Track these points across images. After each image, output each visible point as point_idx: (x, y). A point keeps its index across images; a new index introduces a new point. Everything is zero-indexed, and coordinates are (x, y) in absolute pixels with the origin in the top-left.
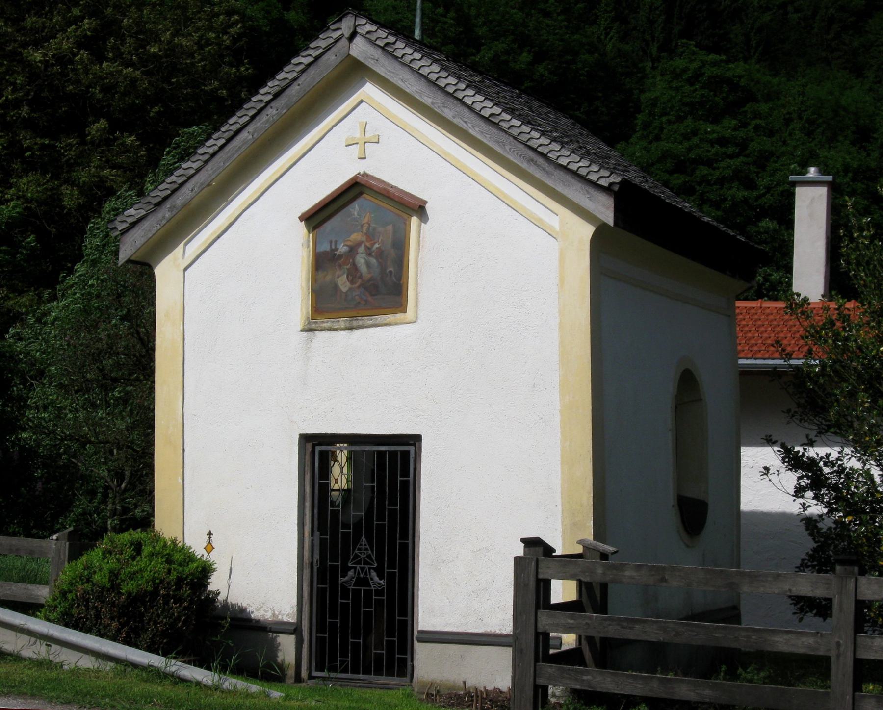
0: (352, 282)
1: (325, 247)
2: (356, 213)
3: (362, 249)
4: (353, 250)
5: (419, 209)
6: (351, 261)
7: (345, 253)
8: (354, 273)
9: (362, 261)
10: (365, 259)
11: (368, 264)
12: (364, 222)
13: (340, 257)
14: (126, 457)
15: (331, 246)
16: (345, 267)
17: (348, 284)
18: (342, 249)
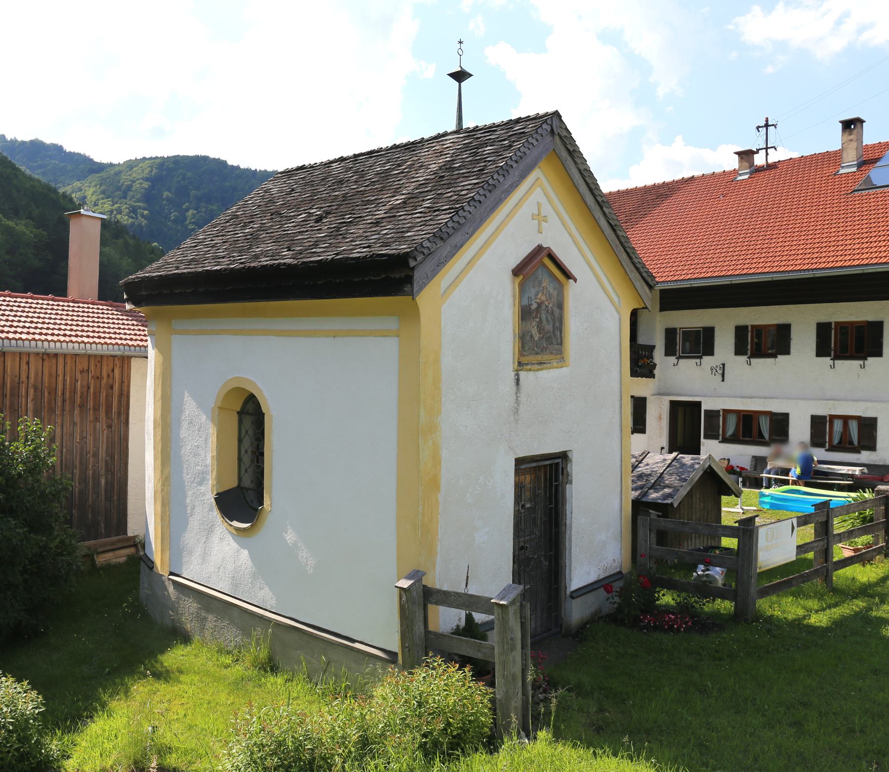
9: (544, 316)
18: (534, 306)
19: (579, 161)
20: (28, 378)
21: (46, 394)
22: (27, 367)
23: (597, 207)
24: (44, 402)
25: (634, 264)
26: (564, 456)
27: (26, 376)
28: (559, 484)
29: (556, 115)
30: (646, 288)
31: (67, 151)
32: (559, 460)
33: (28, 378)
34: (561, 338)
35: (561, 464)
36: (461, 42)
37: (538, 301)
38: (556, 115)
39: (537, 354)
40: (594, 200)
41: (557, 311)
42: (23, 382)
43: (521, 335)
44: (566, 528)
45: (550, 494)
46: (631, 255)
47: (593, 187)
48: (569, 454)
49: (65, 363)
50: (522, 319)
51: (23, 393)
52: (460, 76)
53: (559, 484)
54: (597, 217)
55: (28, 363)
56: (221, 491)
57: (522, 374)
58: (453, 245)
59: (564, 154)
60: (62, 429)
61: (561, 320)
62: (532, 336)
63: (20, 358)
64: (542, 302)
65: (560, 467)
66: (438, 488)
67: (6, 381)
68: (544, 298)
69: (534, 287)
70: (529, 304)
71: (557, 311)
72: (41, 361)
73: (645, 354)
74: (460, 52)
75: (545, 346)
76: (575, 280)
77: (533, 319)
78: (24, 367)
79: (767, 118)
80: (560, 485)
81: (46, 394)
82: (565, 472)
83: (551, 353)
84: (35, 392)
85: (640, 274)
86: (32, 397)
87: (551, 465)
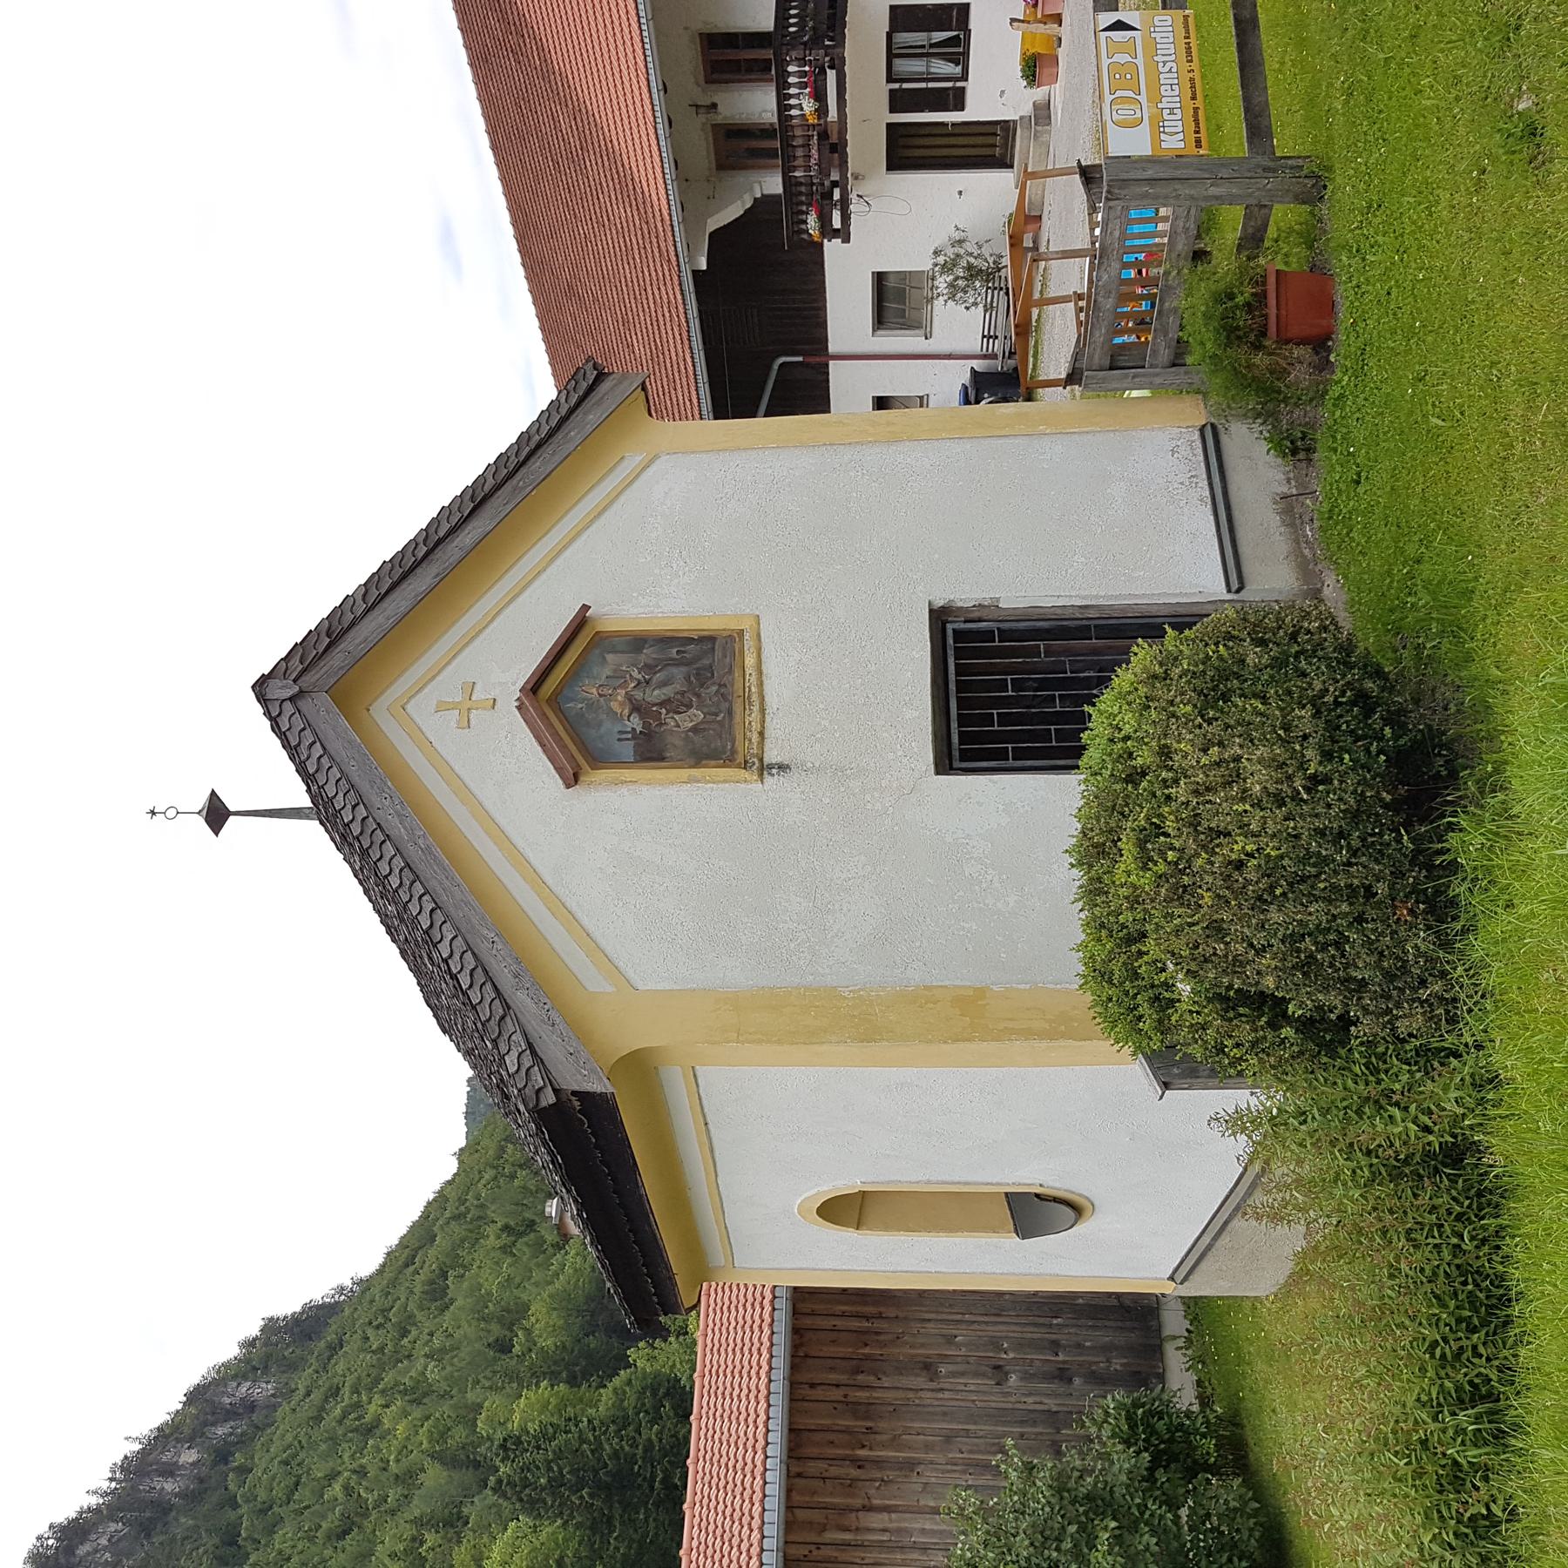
0: (689, 706)
1: (627, 750)
2: (580, 706)
3: (638, 695)
4: (636, 708)
5: (580, 622)
6: (654, 709)
7: (641, 719)
8: (676, 705)
9: (656, 692)
10: (654, 690)
11: (664, 684)
12: (596, 693)
13: (646, 725)
15: (628, 739)
16: (663, 716)
17: (693, 711)
18: (636, 723)
19: (349, 617)
20: (837, 1386)
21: (867, 1351)
22: (819, 1388)
23: (438, 553)
24: (882, 1355)
25: (552, 433)
26: (939, 617)
27: (834, 1388)
28: (998, 629)
29: (261, 688)
30: (605, 386)
31: (471, 1073)
32: (950, 627)
33: (837, 1386)
34: (702, 639)
35: (956, 626)
36: (153, 813)
37: (626, 712)
38: (261, 688)
39: (730, 712)
40: (424, 565)
41: (649, 654)
42: (846, 1396)
43: (692, 762)
44: (1093, 606)
45: (1079, 336)
46: (533, 444)
47: (398, 572)
48: (939, 603)
49: (813, 1314)
50: (662, 759)
51: (868, 1394)
52: (216, 814)
53: (998, 629)
54: (458, 555)
55: (813, 1386)
56: (1012, 1227)
57: (771, 756)
58: (514, 981)
59: (337, 659)
60: (929, 1320)
61: (666, 640)
62: (695, 729)
63: (803, 1400)
64: (629, 697)
65: (962, 626)
66: (981, 992)
67: (844, 1428)
68: (621, 695)
69: (600, 725)
70: (634, 738)
71: (649, 654)
72: (810, 1361)
73: (795, 8)
74: (171, 813)
75: (715, 688)
76: (585, 608)
77: (661, 724)
78: (819, 1393)
79: (127, 1439)
80: (1001, 625)
81: (867, 1351)
82: (976, 615)
83: (731, 671)
84: (862, 1372)
85: (572, 411)
86: (872, 1378)
87: (959, 653)
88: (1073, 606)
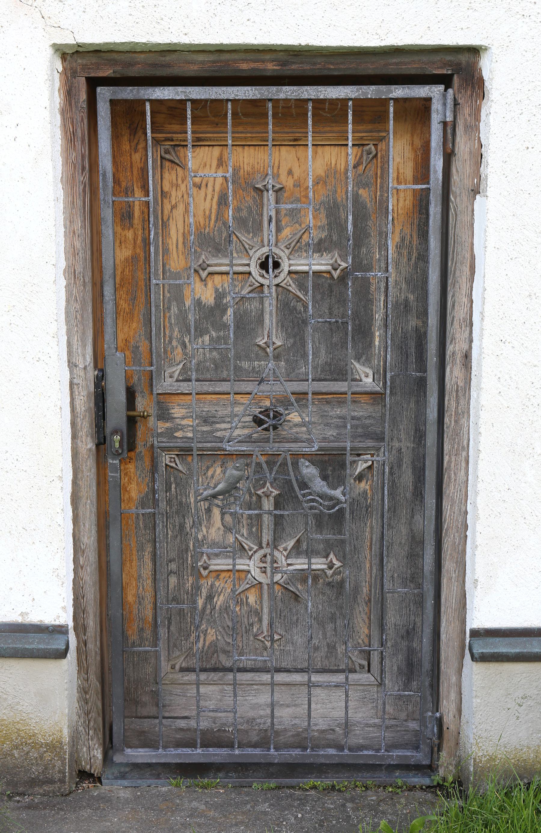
14: (218, 577)
35: (436, 106)
88: (471, 341)
